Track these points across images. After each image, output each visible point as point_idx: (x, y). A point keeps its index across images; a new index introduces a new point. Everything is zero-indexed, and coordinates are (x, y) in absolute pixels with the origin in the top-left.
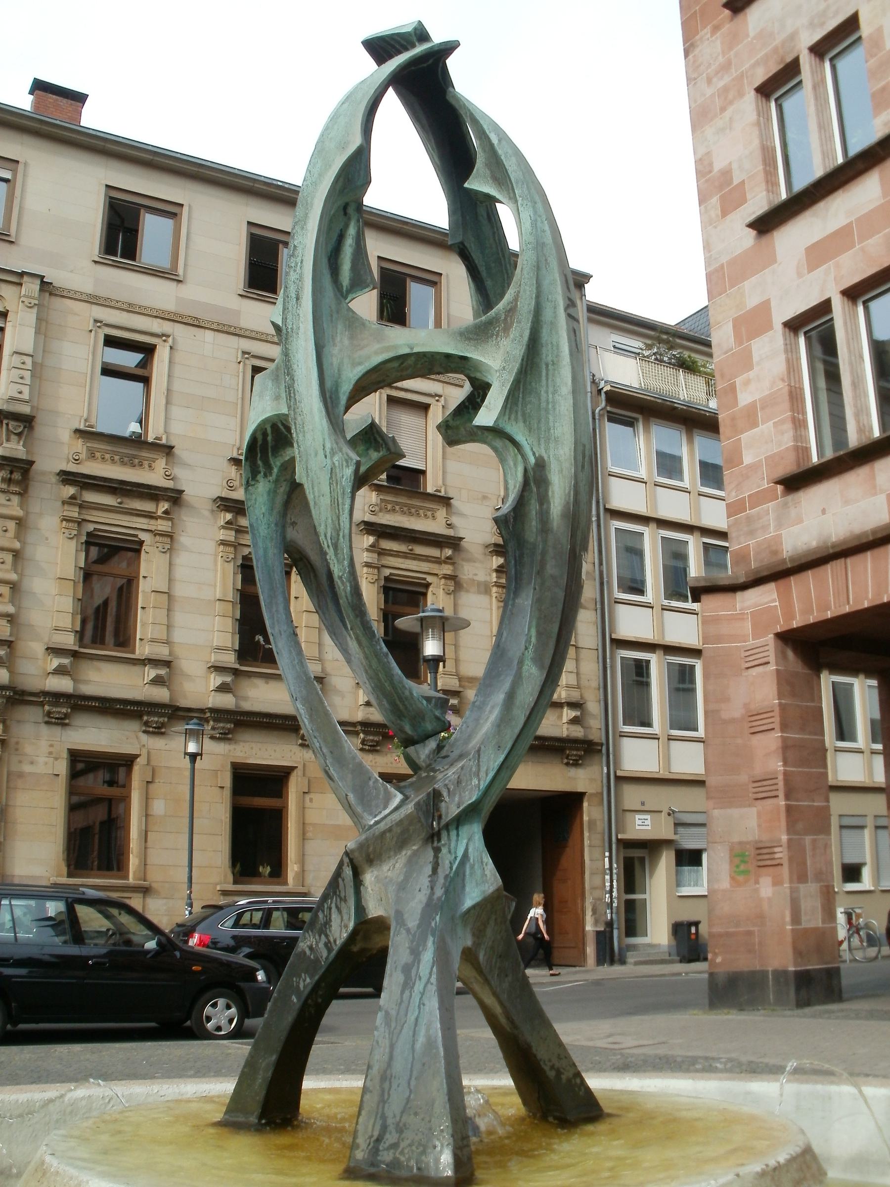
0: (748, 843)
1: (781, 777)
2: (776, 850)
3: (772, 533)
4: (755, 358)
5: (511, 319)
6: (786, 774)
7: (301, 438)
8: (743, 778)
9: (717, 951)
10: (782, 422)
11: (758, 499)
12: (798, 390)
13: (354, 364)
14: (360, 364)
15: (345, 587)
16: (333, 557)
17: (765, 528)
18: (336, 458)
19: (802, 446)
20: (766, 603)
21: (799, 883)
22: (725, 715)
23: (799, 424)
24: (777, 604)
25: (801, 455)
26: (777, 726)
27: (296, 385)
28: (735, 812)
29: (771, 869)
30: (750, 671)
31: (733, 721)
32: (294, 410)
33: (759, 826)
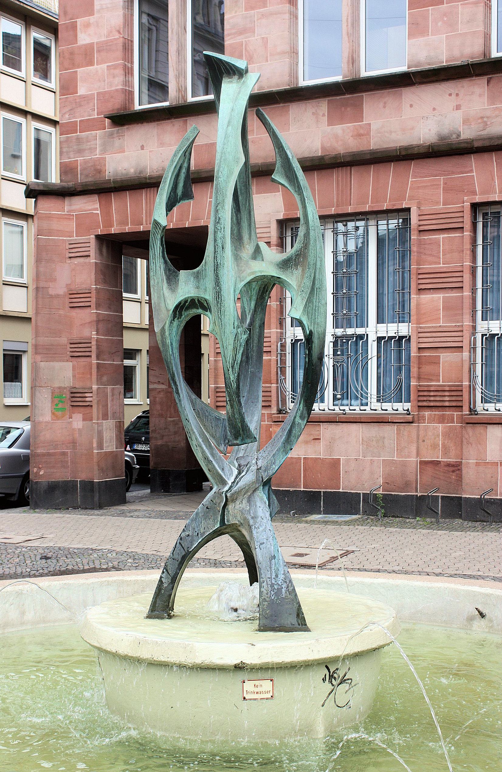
0: (65, 388)
1: (94, 343)
2: (87, 395)
3: (97, 155)
4: (97, 7)
5: (298, 260)
6: (97, 340)
7: (223, 317)
8: (64, 340)
9: (40, 466)
10: (115, 67)
11: (88, 125)
12: (130, 42)
13: (241, 281)
14: (243, 281)
15: (234, 385)
16: (231, 372)
17: (92, 150)
18: (239, 330)
19: (129, 90)
20: (89, 210)
21: (102, 420)
22: (51, 292)
23: (128, 72)
24: (99, 212)
25: (127, 98)
26: (93, 304)
27: (222, 292)
28: (57, 365)
29: (82, 409)
30: (73, 260)
31: (57, 296)
32: (220, 304)
33: (74, 376)
